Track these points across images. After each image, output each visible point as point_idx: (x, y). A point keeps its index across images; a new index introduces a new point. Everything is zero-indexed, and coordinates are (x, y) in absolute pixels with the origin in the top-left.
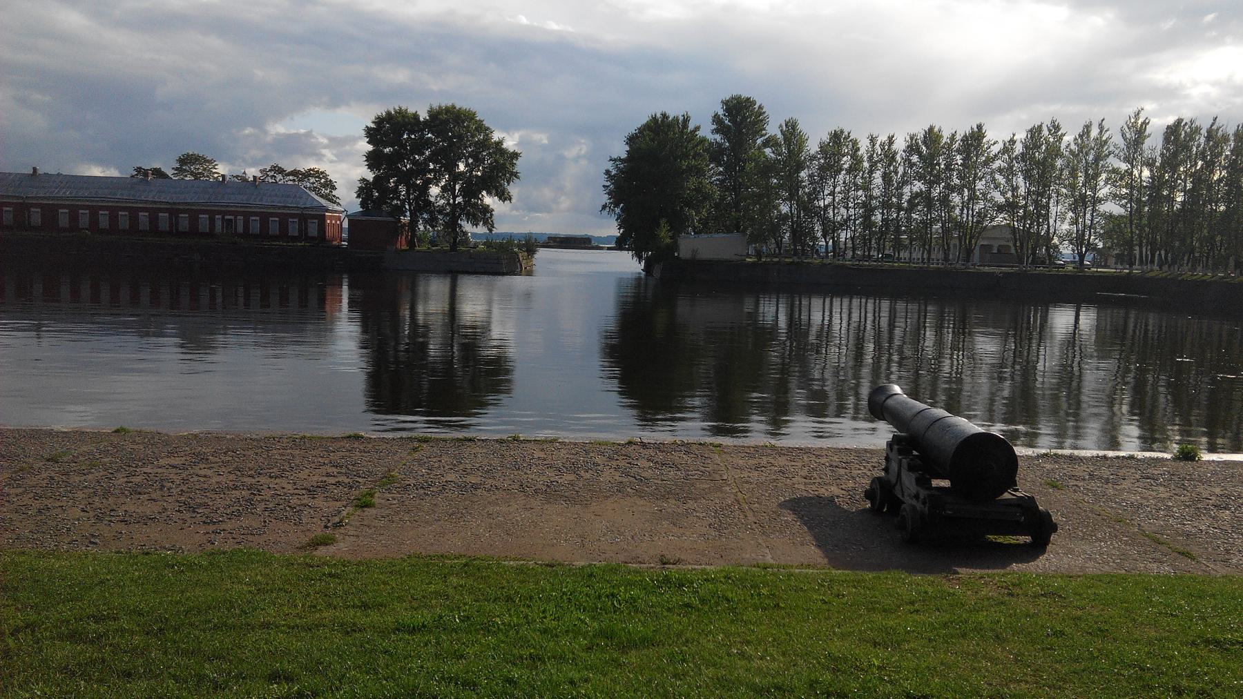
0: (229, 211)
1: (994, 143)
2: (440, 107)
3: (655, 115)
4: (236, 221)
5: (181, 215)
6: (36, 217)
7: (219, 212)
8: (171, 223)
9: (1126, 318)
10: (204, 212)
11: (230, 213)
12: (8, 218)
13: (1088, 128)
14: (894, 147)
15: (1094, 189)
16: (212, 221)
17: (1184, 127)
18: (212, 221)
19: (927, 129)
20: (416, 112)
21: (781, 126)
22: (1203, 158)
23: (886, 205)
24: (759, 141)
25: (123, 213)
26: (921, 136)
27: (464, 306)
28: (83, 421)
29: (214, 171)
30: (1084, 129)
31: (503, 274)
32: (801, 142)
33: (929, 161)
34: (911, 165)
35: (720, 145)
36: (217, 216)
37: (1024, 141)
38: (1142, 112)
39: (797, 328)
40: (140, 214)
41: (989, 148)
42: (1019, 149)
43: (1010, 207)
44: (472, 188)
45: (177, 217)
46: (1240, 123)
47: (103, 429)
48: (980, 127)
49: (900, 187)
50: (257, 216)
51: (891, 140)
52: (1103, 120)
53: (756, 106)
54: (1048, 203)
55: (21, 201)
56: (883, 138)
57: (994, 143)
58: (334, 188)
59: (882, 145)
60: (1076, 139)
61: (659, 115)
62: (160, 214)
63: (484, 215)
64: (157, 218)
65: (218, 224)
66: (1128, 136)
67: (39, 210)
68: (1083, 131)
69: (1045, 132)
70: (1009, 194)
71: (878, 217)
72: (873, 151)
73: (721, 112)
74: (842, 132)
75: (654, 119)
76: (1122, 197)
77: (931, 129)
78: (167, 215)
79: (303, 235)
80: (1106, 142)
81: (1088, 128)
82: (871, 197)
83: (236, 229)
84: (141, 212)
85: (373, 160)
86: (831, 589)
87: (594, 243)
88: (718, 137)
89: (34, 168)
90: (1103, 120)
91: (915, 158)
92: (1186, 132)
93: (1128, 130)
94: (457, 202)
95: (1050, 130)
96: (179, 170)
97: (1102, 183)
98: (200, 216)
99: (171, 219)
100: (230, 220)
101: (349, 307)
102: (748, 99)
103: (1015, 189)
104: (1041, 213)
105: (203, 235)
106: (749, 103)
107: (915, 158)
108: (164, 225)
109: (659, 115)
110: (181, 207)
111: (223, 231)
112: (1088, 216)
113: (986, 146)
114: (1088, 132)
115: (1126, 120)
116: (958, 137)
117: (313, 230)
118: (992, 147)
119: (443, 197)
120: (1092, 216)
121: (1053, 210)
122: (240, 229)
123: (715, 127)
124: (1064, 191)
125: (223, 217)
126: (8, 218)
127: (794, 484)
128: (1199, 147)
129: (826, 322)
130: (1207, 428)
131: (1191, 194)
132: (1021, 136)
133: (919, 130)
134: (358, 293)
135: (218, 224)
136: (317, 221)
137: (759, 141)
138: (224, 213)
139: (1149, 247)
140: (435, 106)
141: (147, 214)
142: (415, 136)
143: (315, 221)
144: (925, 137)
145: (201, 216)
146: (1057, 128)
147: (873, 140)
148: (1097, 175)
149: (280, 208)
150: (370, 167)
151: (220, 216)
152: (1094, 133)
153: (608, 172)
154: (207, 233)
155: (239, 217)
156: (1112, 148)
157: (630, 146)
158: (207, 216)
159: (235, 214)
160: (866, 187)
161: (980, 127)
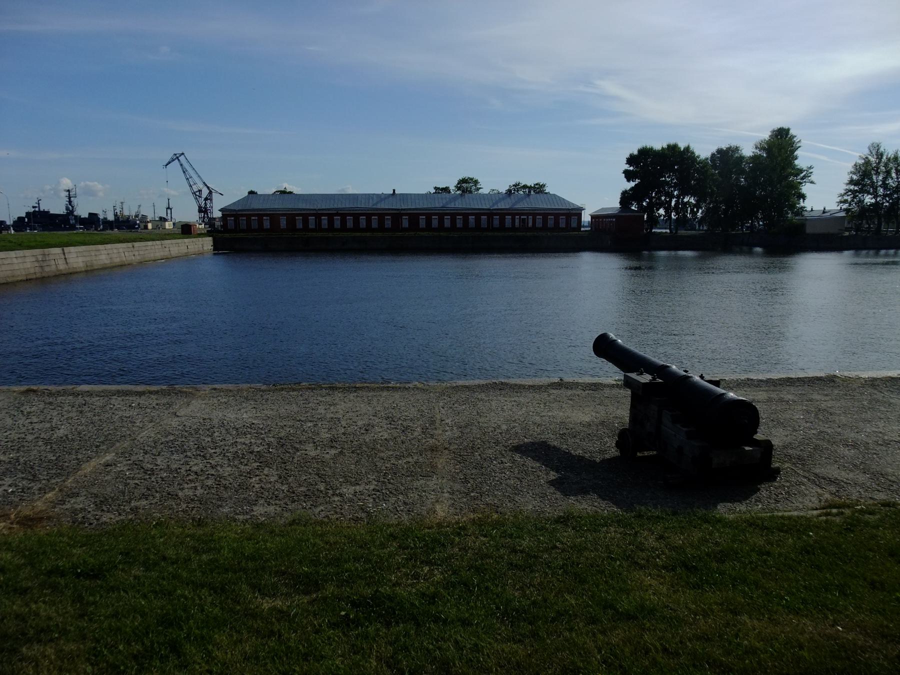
6: (283, 223)
10: (509, 214)
16: (513, 220)
18: (513, 220)
25: (388, 217)
28: (160, 364)
36: (516, 217)
40: (470, 217)
45: (493, 218)
52: (139, 206)
55: (568, 212)
78: (486, 217)
79: (568, 228)
86: (862, 471)
94: (217, 214)
99: (316, 219)
109: (627, 167)
110: (495, 212)
111: (316, 226)
122: (530, 224)
123: (853, 170)
125: (520, 217)
135: (517, 221)
138: (520, 214)
142: (642, 162)
150: (628, 181)
151: (518, 217)
155: (530, 217)
159: (528, 214)
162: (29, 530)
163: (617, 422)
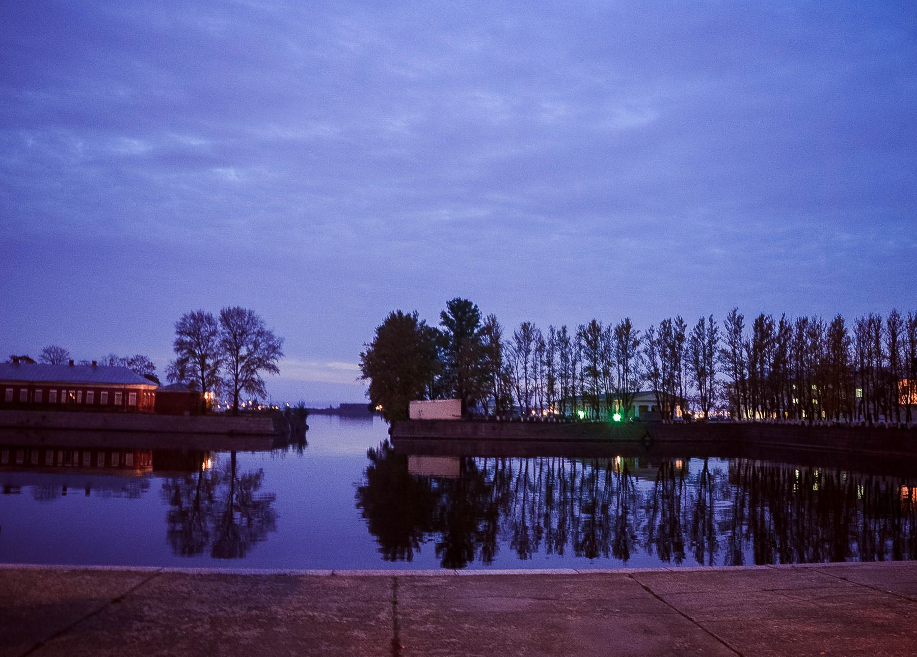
1: (638, 332)
3: (393, 312)
9: (497, 462)
10: (53, 388)
13: (702, 321)
14: (567, 335)
15: (710, 364)
16: (84, 395)
17: (765, 321)
18: (59, 394)
22: (779, 342)
23: (564, 376)
24: (476, 331)
26: (587, 326)
30: (699, 322)
33: (593, 345)
34: (581, 347)
35: (447, 333)
36: (63, 391)
37: (659, 330)
38: (737, 310)
39: (503, 477)
41: (635, 335)
42: (656, 337)
43: (654, 375)
44: (252, 364)
45: (34, 392)
48: (627, 320)
49: (574, 363)
54: (679, 375)
56: (559, 328)
57: (638, 332)
58: (154, 368)
59: (559, 333)
60: (694, 329)
61: (396, 312)
63: (254, 386)
64: (49, 392)
66: (730, 327)
68: (699, 324)
69: (673, 324)
70: (652, 368)
72: (553, 338)
73: (446, 310)
75: (393, 315)
76: (729, 370)
80: (716, 331)
81: (702, 321)
82: (554, 371)
88: (446, 328)
90: (712, 315)
91: (584, 342)
92: (766, 324)
93: (729, 322)
95: (676, 323)
97: (715, 360)
102: (466, 301)
103: (654, 364)
106: (467, 304)
108: (23, 398)
109: (396, 312)
112: (708, 383)
113: (632, 334)
114: (703, 324)
115: (727, 316)
116: (612, 328)
118: (636, 335)
120: (711, 383)
121: (683, 380)
123: (442, 320)
124: (691, 365)
127: (899, 638)
128: (601, 338)
129: (523, 471)
131: (775, 366)
132: (657, 327)
137: (476, 331)
139: (751, 405)
140: (226, 307)
143: (133, 394)
144: (590, 327)
145: (22, 390)
146: (681, 322)
147: (552, 331)
148: (711, 354)
149: (108, 384)
152: (707, 325)
153: (362, 355)
155: (79, 392)
156: (719, 335)
157: (379, 335)
160: (549, 363)
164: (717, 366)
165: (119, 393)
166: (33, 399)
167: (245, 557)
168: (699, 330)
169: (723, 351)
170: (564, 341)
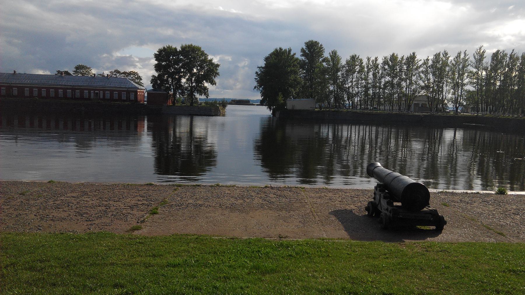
0: (97, 89)
1: (420, 61)
2: (186, 45)
3: (277, 49)
4: (99, 93)
5: (76, 91)
6: (15, 92)
7: (93, 90)
8: (72, 94)
10: (86, 89)
11: (97, 90)
12: (3, 92)
13: (459, 54)
14: (378, 62)
16: (90, 93)
17: (500, 54)
18: (90, 93)
19: (391, 55)
20: (176, 47)
21: (330, 53)
22: (508, 67)
23: (374, 87)
24: (321, 60)
25: (52, 90)
26: (389, 57)
27: (196, 129)
29: (90, 72)
30: (458, 54)
31: (212, 116)
32: (338, 60)
33: (392, 68)
34: (385, 70)
35: (304, 61)
36: (92, 91)
38: (482, 47)
39: (337, 139)
40: (59, 90)
42: (430, 63)
43: (427, 87)
44: (200, 80)
45: (75, 92)
46: (524, 52)
47: (44, 181)
48: (414, 54)
49: (380, 79)
50: (108, 91)
51: (376, 59)
53: (319, 45)
54: (443, 86)
56: (373, 58)
57: (420, 61)
58: (141, 79)
59: (373, 61)
60: (454, 59)
61: (278, 49)
62: (68, 90)
63: (204, 91)
64: (66, 92)
65: (92, 95)
67: (17, 89)
68: (458, 55)
69: (441, 56)
70: (426, 82)
71: (371, 92)
72: (369, 64)
73: (304, 47)
74: (356, 56)
75: (276, 50)
76: (474, 83)
77: (393, 54)
78: (70, 91)
79: (128, 99)
80: (467, 60)
81: (459, 54)
82: (368, 83)
83: (99, 97)
84: (59, 89)
85: (158, 67)
86: (351, 249)
87: (251, 103)
88: (303, 58)
89: (14, 71)
90: (466, 51)
91: (386, 67)
93: (476, 55)
95: (443, 55)
96: (76, 72)
97: (465, 77)
98: (85, 91)
99: (72, 92)
100: (97, 93)
101: (148, 130)
102: (316, 42)
103: (429, 80)
104: (440, 90)
105: (86, 99)
106: (316, 43)
107: (386, 67)
108: (69, 95)
109: (278, 49)
110: (76, 87)
111: (94, 97)
112: (460, 91)
113: (416, 62)
114: (460, 56)
115: (475, 51)
116: (405, 58)
117: (132, 97)
118: (419, 62)
119: (187, 83)
120: (461, 91)
121: (445, 88)
122: (101, 97)
123: (302, 53)
124: (449, 80)
125: (94, 92)
126: (3, 92)
128: (506, 62)
129: (349, 136)
130: (510, 181)
131: (503, 82)
132: (431, 57)
133: (388, 55)
134: (151, 123)
135: (92, 95)
136: (134, 93)
137: (321, 60)
138: (95, 90)
139: (485, 104)
140: (184, 45)
141: (62, 90)
142: (175, 57)
143: (133, 93)
144: (391, 58)
145: (85, 91)
146: (447, 54)
147: (369, 59)
148: (463, 74)
149: (118, 88)
150: (156, 70)
151: (93, 91)
153: (257, 73)
154: (87, 98)
155: (101, 92)
156: (470, 63)
157: (266, 62)
158: (88, 91)
159: (99, 90)
160: (366, 79)
161: (414, 54)
162: (466, 77)
163: (370, 107)
164: (466, 81)
165: (52, 90)
166: (75, 94)
167: (445, 223)
168: (457, 60)
169: (471, 72)
170: (376, 66)
